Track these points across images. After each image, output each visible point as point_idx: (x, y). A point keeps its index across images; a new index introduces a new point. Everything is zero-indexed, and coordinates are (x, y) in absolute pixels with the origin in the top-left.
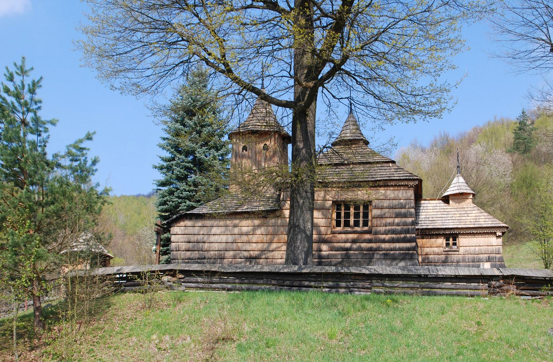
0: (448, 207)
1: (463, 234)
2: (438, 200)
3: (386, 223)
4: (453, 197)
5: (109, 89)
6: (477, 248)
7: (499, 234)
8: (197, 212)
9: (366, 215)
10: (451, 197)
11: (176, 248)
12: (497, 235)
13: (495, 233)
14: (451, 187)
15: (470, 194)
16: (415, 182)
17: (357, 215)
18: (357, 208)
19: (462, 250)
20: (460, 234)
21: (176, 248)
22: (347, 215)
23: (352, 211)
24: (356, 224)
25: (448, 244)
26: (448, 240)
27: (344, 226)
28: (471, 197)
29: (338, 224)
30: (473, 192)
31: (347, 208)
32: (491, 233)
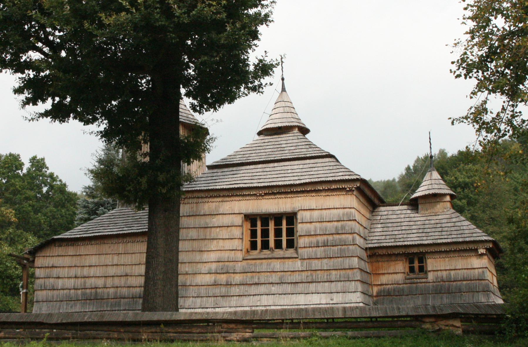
0: (416, 215)
1: (432, 252)
2: (402, 205)
3: (318, 242)
4: (423, 201)
5: (453, 76)
6: (452, 273)
7: (482, 251)
8: (69, 237)
9: (291, 232)
10: (420, 201)
11: (41, 287)
12: (480, 253)
13: (476, 250)
14: (422, 185)
15: (445, 195)
16: (355, 184)
17: (278, 233)
18: (278, 223)
19: (431, 276)
20: (427, 252)
21: (41, 287)
22: (265, 233)
23: (272, 227)
24: (278, 245)
25: (412, 270)
26: (411, 262)
27: (287, 247)
28: (448, 198)
29: (253, 246)
30: (452, 193)
31: (278, 223)
32: (471, 250)
